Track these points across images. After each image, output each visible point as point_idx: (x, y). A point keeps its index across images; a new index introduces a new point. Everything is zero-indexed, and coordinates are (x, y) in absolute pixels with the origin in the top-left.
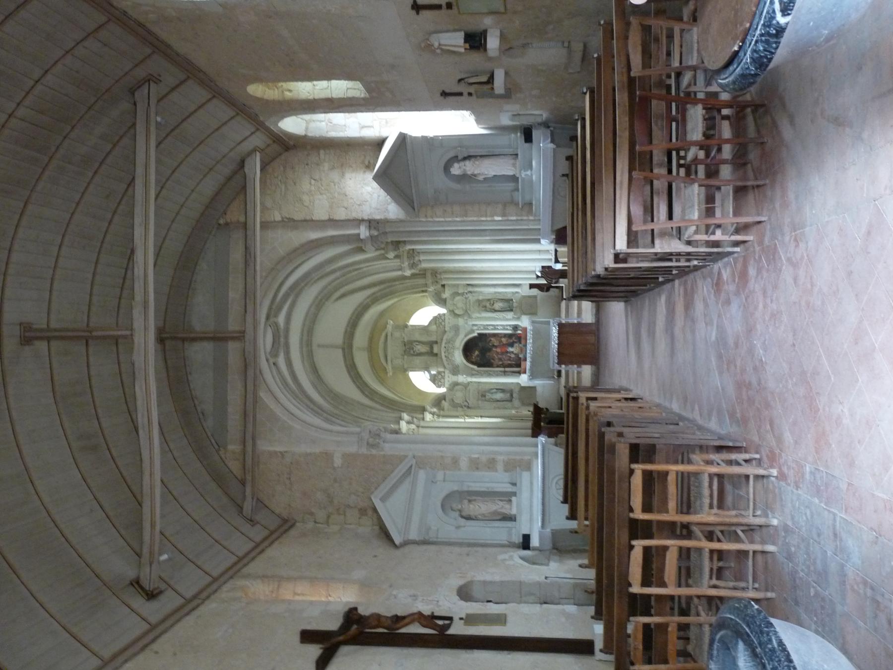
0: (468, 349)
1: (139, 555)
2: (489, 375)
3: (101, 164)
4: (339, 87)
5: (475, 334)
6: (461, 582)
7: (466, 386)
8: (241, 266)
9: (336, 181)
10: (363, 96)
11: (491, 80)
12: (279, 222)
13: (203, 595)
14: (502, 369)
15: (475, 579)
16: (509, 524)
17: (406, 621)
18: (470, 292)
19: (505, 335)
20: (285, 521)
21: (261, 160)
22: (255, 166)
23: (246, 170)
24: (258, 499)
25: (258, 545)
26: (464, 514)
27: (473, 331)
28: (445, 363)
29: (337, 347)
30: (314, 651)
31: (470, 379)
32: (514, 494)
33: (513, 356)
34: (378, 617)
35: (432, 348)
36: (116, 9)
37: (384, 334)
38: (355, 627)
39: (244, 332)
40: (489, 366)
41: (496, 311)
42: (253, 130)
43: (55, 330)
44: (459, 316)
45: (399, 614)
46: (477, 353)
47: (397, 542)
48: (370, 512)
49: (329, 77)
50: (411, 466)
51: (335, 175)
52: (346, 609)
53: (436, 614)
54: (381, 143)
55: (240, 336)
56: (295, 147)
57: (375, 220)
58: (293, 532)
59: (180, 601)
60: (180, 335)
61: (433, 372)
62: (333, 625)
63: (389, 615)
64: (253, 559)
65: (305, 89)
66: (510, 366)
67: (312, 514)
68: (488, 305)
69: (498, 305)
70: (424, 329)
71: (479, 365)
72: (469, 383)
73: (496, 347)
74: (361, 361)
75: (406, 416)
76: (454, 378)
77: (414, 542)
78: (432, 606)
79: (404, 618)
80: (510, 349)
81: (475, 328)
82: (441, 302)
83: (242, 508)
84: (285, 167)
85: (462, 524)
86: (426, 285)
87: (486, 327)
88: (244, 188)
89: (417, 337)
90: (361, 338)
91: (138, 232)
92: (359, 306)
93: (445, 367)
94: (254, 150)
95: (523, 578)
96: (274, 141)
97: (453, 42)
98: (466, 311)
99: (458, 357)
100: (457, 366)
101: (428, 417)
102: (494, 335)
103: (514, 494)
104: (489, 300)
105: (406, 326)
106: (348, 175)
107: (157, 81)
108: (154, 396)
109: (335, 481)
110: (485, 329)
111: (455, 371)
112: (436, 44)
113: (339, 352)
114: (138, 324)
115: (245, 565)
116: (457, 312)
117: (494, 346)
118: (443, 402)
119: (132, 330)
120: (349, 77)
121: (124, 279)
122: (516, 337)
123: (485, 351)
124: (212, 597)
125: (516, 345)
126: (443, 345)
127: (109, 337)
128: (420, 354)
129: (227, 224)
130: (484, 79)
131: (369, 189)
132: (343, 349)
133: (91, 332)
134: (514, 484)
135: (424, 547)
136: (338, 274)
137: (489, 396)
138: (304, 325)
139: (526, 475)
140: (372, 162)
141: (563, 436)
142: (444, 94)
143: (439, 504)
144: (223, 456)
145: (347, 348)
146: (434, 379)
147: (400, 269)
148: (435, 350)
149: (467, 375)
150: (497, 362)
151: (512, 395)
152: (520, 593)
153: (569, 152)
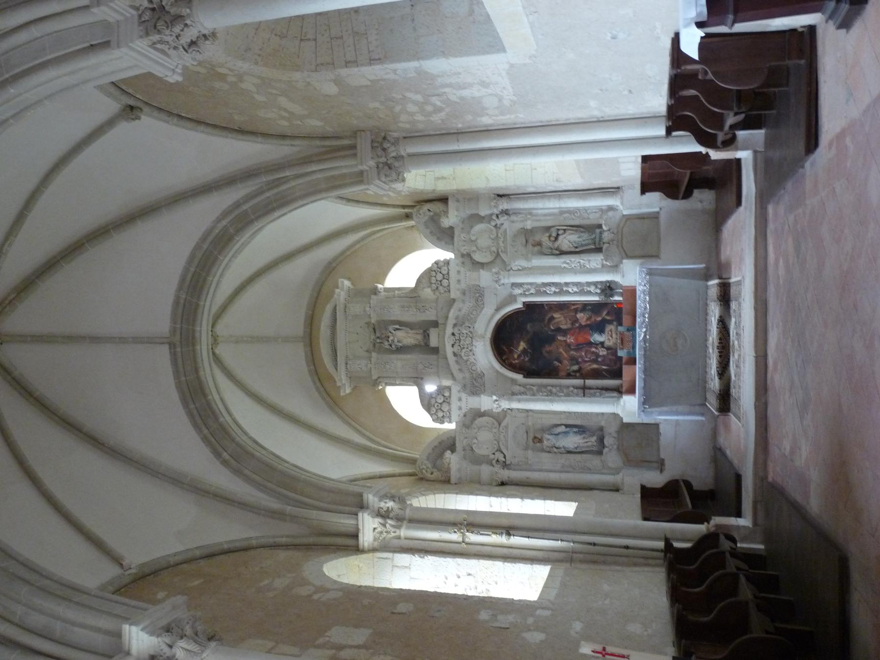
0: (503, 338)
2: (551, 394)
5: (518, 305)
7: (499, 418)
14: (579, 382)
18: (506, 212)
19: (585, 307)
27: (512, 299)
31: (505, 405)
33: (603, 352)
35: (426, 336)
41: (563, 253)
44: (482, 265)
46: (522, 345)
61: (431, 388)
66: (596, 374)
68: (546, 240)
69: (567, 240)
70: (411, 296)
71: (529, 374)
72: (505, 412)
73: (564, 332)
79: (582, 561)
80: (597, 338)
81: (517, 291)
87: (540, 289)
89: (396, 313)
98: (498, 255)
99: (483, 355)
100: (482, 375)
102: (562, 307)
104: (548, 229)
105: (375, 291)
110: (539, 293)
111: (476, 385)
116: (478, 257)
117: (559, 330)
122: (612, 310)
123: (540, 341)
125: (609, 327)
126: (449, 330)
128: (401, 350)
132: (172, 346)
137: (549, 440)
146: (427, 403)
148: (434, 342)
150: (567, 366)
151: (601, 440)
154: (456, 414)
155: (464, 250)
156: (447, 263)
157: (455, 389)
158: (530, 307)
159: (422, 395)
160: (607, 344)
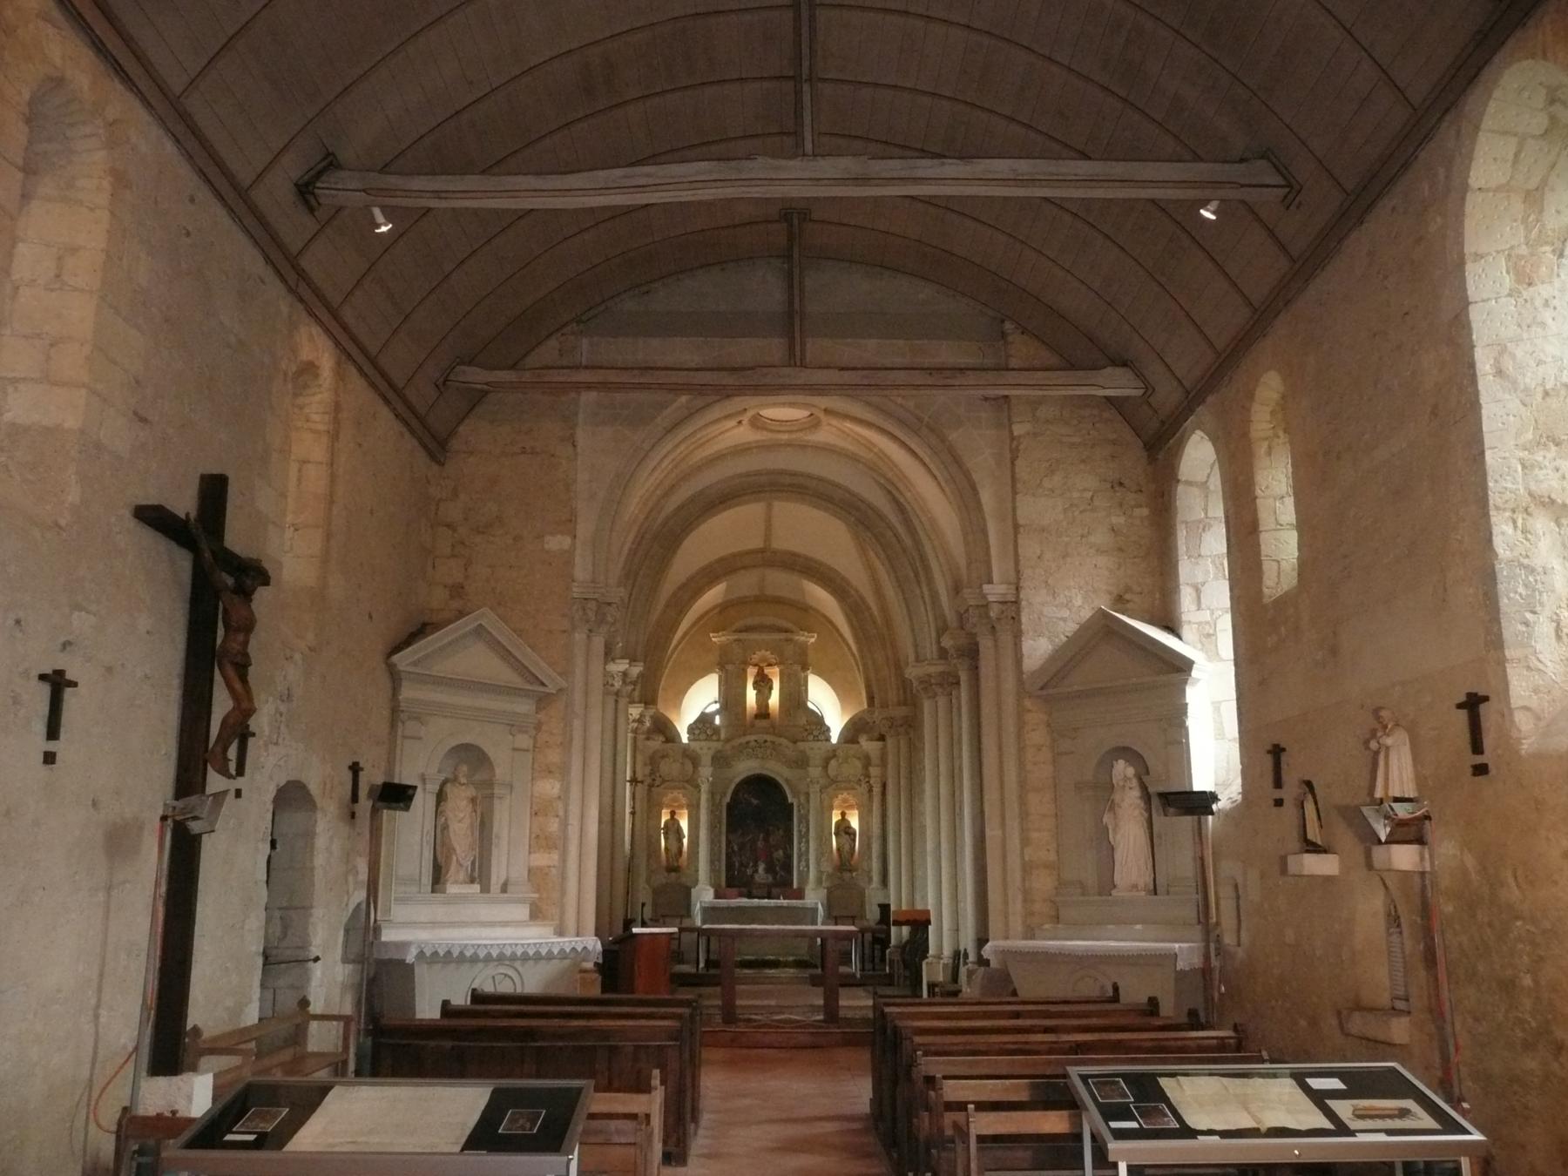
1: (385, 169)
3: (1125, 100)
4: (1283, 547)
6: (314, 788)
8: (927, 362)
9: (1092, 539)
10: (1265, 590)
11: (1312, 848)
12: (1011, 432)
13: (303, 289)
15: (319, 815)
16: (427, 879)
17: (238, 686)
18: (870, 791)
20: (443, 444)
21: (1127, 398)
22: (1117, 384)
23: (1109, 370)
24: (487, 393)
25: (399, 393)
26: (448, 787)
28: (737, 742)
29: (767, 537)
30: (184, 504)
31: (704, 788)
32: (485, 889)
33: (749, 872)
34: (248, 627)
36: (1440, 120)
37: (786, 624)
38: (230, 581)
39: (803, 366)
40: (729, 825)
42: (1187, 384)
43: (812, 18)
45: (251, 669)
47: (395, 658)
48: (456, 604)
49: (1304, 525)
50: (543, 684)
51: (1101, 537)
52: (266, 565)
53: (251, 741)
54: (1172, 628)
55: (795, 359)
56: (1152, 459)
57: (1018, 612)
58: (421, 455)
59: (294, 243)
60: (796, 250)
61: (717, 721)
62: (236, 538)
63: (253, 648)
64: (373, 385)
65: (1276, 485)
67: (455, 494)
71: (730, 807)
72: (697, 787)
73: (766, 840)
74: (746, 583)
75: (636, 670)
76: (706, 759)
77: (395, 690)
78: (267, 730)
79: (244, 679)
80: (761, 867)
81: (802, 799)
82: (854, 731)
83: (470, 363)
84: (1114, 443)
85: (428, 786)
86: (884, 705)
87: (805, 819)
88: (1071, 366)
90: (780, 582)
91: (1001, 167)
92: (843, 579)
93: (728, 740)
94: (1149, 389)
95: (318, 912)
96: (1163, 423)
97: (1394, 773)
99: (745, 767)
100: (728, 765)
101: (635, 711)
103: (485, 889)
105: (805, 668)
106: (1102, 561)
107: (1287, 203)
108: (686, 196)
109: (517, 538)
111: (720, 760)
112: (1389, 741)
113: (756, 543)
114: (829, 167)
115: (360, 369)
116: (833, 763)
117: (768, 834)
118: (662, 738)
119: (815, 155)
120: (1304, 565)
121: (903, 147)
122: (783, 882)
124: (300, 306)
126: (769, 738)
127: (798, 115)
129: (1003, 335)
130: (1313, 834)
131: (1078, 601)
132: (762, 551)
133: (810, 80)
134: (504, 889)
135: (386, 713)
136: (908, 542)
138: (809, 476)
139: (522, 912)
140: (1129, 606)
141: (596, 992)
142: (1277, 752)
143: (467, 739)
144: (567, 330)
145: (768, 558)
146: (704, 720)
147: (917, 659)
149: (712, 784)
152: (286, 908)
153: (1167, 1009)
154: (696, 746)
155: (840, 753)
156: (828, 739)
157: (718, 745)
158: (788, 810)
159: (713, 715)
160: (756, 877)
